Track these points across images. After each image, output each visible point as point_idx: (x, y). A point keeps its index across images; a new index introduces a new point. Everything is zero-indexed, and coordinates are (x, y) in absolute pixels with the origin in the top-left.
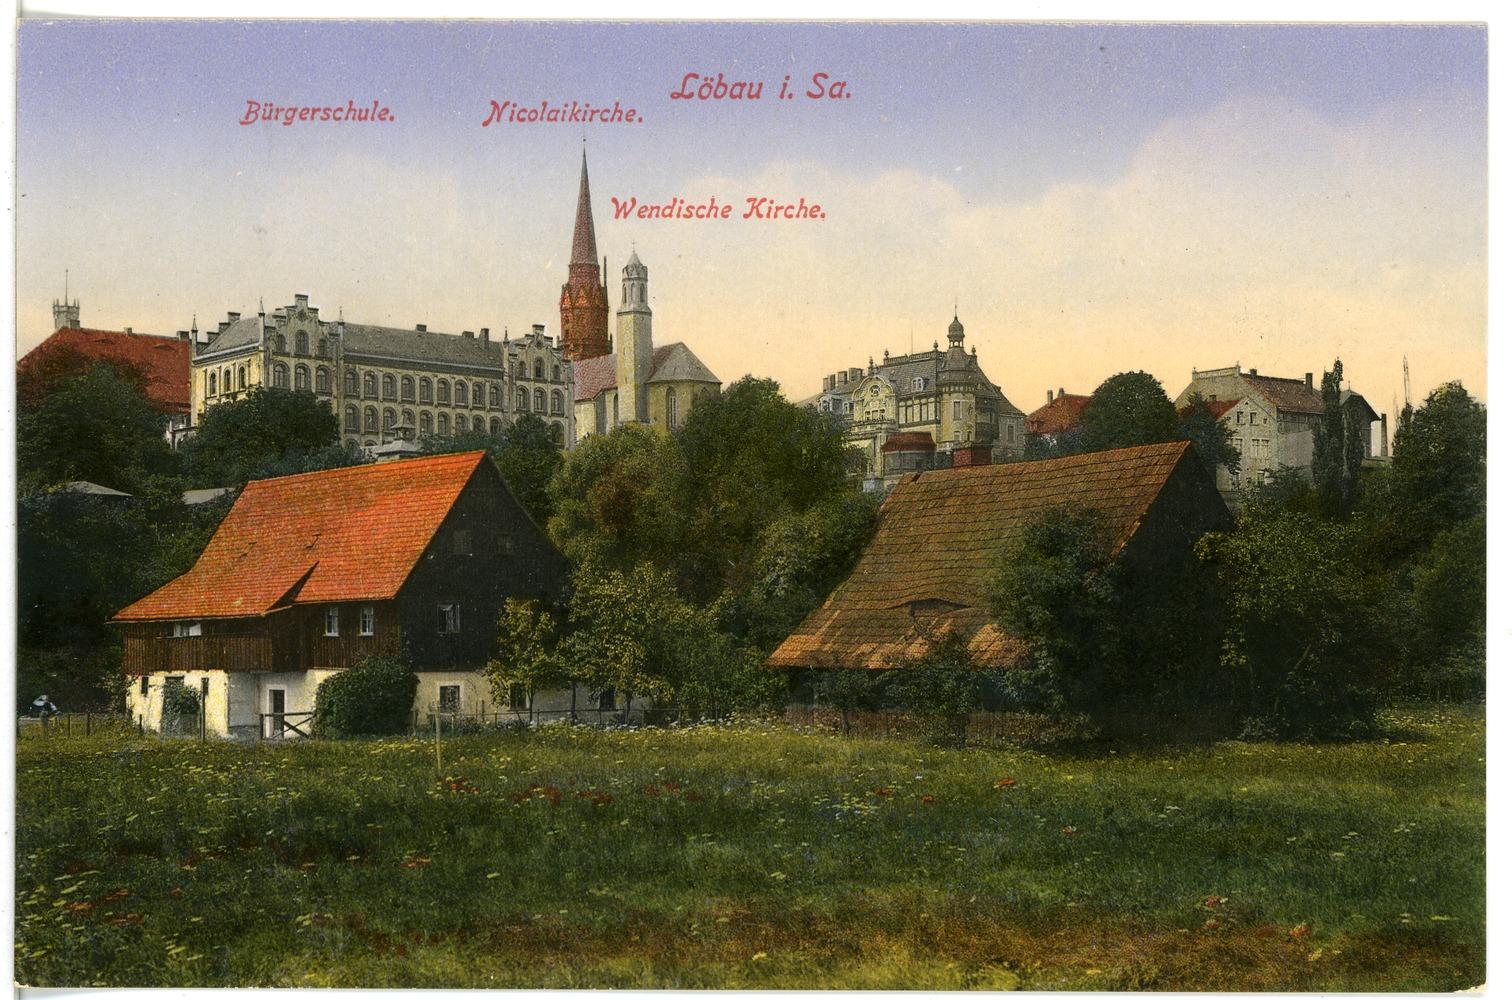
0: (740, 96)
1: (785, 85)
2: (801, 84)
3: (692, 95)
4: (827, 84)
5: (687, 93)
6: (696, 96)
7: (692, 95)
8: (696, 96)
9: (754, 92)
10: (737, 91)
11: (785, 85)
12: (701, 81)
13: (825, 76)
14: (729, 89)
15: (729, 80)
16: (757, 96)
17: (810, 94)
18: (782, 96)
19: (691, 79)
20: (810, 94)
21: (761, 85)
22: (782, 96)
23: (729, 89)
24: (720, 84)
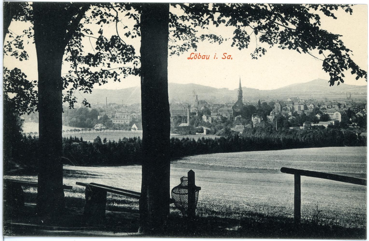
0: (204, 58)
1: (215, 56)
2: (221, 55)
3: (192, 58)
4: (226, 55)
5: (191, 57)
6: (193, 58)
7: (192, 58)
8: (193, 58)
9: (207, 58)
10: (203, 57)
11: (215, 56)
12: (194, 55)
13: (226, 54)
14: (197, 58)
15: (202, 55)
16: (208, 58)
17: (223, 58)
18: (214, 58)
19: (192, 54)
20: (223, 58)
21: (209, 56)
22: (214, 58)
23: (197, 58)
24: (199, 55)
